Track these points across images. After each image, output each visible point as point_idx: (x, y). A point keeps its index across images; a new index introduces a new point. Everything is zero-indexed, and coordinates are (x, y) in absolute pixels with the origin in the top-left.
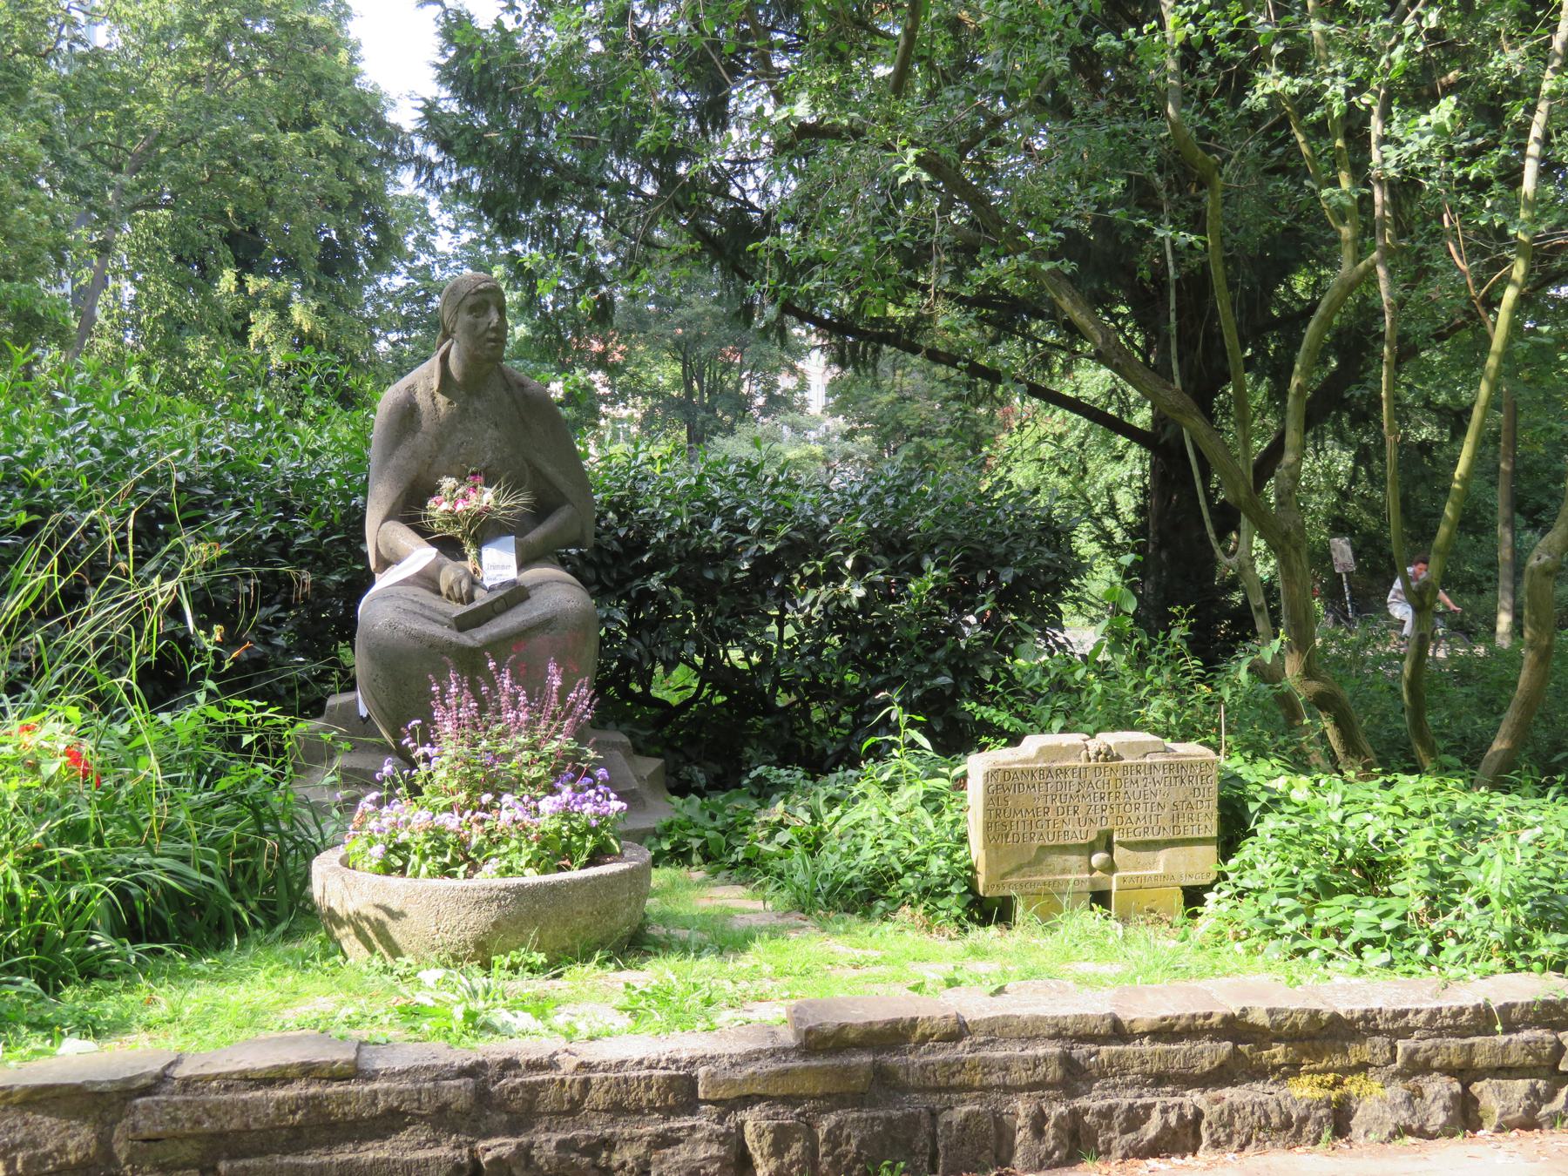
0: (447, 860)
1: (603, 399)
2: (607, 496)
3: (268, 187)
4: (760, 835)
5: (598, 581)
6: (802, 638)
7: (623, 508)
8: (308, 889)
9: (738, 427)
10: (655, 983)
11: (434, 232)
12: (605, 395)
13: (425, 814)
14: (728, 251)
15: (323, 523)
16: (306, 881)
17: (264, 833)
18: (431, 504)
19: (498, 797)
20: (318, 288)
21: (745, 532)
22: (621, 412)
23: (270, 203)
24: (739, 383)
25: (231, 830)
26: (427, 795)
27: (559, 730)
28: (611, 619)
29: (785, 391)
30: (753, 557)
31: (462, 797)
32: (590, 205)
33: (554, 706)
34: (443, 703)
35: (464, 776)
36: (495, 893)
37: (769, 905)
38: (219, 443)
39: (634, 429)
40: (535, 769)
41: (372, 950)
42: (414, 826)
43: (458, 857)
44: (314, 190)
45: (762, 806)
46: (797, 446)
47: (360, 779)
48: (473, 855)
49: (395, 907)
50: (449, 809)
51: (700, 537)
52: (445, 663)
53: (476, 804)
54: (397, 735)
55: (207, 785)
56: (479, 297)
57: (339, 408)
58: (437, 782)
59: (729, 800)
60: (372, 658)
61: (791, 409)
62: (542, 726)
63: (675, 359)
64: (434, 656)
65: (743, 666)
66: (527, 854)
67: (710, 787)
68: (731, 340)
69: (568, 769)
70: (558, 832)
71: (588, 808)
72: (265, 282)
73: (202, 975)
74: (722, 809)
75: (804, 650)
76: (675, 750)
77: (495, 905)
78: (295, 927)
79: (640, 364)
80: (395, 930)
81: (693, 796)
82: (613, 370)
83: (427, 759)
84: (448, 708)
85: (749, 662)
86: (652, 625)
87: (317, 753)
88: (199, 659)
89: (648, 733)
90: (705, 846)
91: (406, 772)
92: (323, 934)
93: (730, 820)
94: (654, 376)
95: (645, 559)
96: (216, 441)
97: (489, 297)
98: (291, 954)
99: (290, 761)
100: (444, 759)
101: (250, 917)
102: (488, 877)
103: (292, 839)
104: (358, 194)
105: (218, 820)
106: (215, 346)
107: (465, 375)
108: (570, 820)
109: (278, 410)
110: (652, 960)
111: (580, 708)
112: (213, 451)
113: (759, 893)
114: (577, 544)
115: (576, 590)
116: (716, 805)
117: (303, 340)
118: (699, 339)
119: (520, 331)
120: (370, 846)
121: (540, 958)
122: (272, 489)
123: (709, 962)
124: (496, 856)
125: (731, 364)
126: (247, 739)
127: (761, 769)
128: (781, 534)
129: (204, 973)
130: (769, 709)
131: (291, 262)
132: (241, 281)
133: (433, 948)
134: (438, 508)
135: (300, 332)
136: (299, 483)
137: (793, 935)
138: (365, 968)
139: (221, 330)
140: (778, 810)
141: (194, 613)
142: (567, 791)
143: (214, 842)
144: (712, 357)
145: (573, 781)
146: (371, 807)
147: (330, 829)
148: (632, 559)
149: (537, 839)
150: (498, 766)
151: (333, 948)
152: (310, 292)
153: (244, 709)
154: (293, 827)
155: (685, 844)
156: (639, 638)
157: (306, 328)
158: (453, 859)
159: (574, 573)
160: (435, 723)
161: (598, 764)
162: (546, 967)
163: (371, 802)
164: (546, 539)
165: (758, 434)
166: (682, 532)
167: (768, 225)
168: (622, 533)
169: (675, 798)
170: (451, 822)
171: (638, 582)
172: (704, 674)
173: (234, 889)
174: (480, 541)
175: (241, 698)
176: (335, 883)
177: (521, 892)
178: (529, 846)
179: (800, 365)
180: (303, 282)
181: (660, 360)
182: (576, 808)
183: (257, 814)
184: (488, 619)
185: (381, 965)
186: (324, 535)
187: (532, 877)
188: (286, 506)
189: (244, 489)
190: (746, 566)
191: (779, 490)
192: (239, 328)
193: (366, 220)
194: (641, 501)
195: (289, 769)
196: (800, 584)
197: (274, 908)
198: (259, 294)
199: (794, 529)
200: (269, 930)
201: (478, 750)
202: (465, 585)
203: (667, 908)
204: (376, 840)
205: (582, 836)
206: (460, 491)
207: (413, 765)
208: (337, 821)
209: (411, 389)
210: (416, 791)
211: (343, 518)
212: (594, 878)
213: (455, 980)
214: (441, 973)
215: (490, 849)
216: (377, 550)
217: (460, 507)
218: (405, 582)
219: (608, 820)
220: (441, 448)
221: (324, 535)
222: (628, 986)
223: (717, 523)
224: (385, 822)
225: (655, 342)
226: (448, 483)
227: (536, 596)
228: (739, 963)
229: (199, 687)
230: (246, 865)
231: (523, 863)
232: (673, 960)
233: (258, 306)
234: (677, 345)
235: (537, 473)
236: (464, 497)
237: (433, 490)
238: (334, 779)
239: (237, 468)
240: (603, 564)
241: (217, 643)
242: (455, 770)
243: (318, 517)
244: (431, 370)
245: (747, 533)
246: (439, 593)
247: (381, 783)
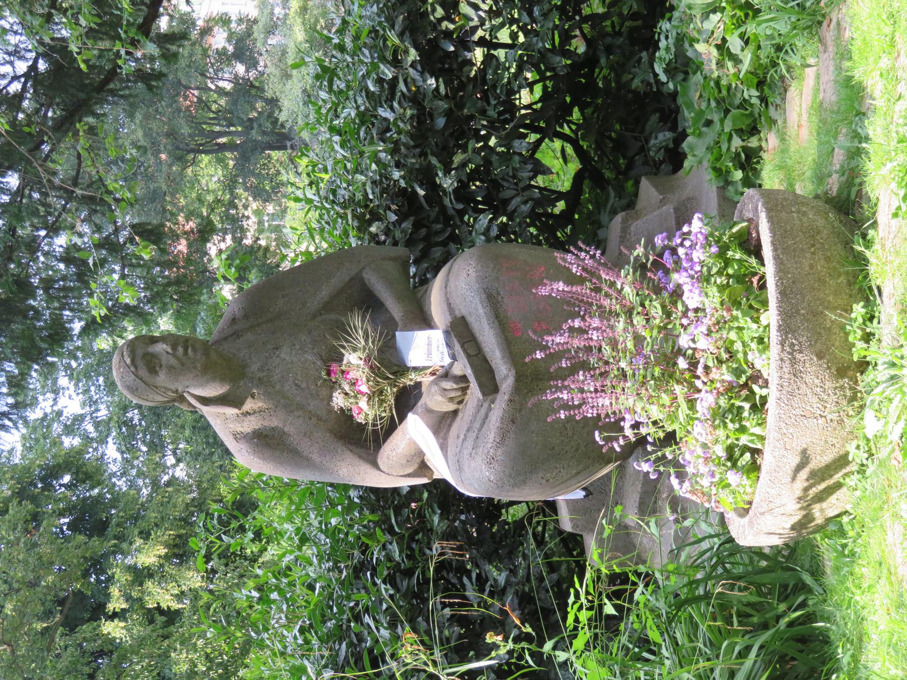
0: (747, 406)
1: (238, 241)
2: (353, 233)
3: (16, 586)
4: (732, 71)
5: (444, 244)
6: (512, 21)
7: (366, 215)
8: (767, 551)
9: (269, 95)
10: (894, 185)
11: (59, 414)
12: (234, 239)
13: (698, 429)
14: (82, 96)
15: (378, 531)
16: (758, 552)
17: (707, 596)
18: (360, 419)
19: (680, 352)
20: (121, 538)
21: (394, 82)
22: (251, 224)
23: (33, 585)
24: (221, 92)
25: (703, 628)
26: (675, 426)
27: (612, 284)
28: (486, 232)
29: (229, 40)
30: (422, 74)
31: (678, 389)
32: (32, 246)
33: (585, 290)
34: (579, 406)
35: (658, 388)
36: (786, 356)
37: (811, 61)
38: (292, 635)
39: (270, 208)
40: (653, 312)
41: (838, 486)
42: (708, 440)
43: (745, 394)
44: (18, 539)
45: (699, 68)
46: (291, 28)
47: (651, 497)
48: (743, 379)
49: (796, 460)
50: (691, 403)
51: (399, 132)
52: (535, 405)
53: (687, 375)
54: (606, 459)
55: (653, 653)
56: (140, 363)
57: (256, 513)
58: (661, 416)
59: (690, 106)
60: (524, 482)
61: (249, 33)
62: (606, 303)
63: (194, 162)
64: (520, 418)
65: (538, 89)
66: (745, 321)
67: (674, 127)
68: (173, 99)
69: (654, 273)
70: (722, 288)
71: (698, 255)
72: (115, 591)
73: (855, 659)
74: (701, 113)
75: (526, 18)
76: (630, 166)
77: (798, 356)
78: (807, 566)
79: (200, 200)
80: (819, 461)
81: (685, 145)
82: (205, 232)
83: (636, 426)
84: (584, 402)
85: (535, 82)
86: (494, 186)
87: (623, 541)
88: (521, 657)
89: (612, 193)
90: (740, 132)
91: (649, 448)
92: (818, 536)
93: (713, 104)
94: (212, 186)
95: (422, 192)
96: (290, 639)
97: (140, 352)
98: (837, 569)
99: (633, 568)
100: (639, 408)
101: (796, 610)
102: (768, 363)
103: (714, 567)
104: (21, 494)
105: (691, 641)
106: (182, 644)
107: (223, 379)
108: (710, 275)
109: (257, 576)
110: (868, 189)
111: (589, 262)
112: (300, 641)
113: (797, 72)
114: (405, 266)
115: (454, 270)
116: (696, 121)
117: (180, 552)
118: (172, 134)
119: (165, 324)
120: (729, 485)
121: (859, 310)
122: (342, 583)
123: (874, 128)
124: (745, 354)
125: (200, 99)
126: (609, 609)
127: (658, 68)
128: (397, 41)
129: (853, 656)
130: (590, 60)
131: (94, 565)
132: (114, 616)
133: (841, 422)
134: (365, 411)
135: (166, 557)
136: (333, 556)
137: (847, 34)
138: (858, 493)
139: (165, 637)
140: (705, 50)
141: (470, 661)
142: (678, 278)
143: (714, 646)
144: (192, 120)
145: (667, 272)
146: (686, 485)
147: (705, 528)
148: (421, 207)
149: (729, 310)
150: (647, 351)
151: (835, 526)
152: (124, 546)
153: (578, 613)
154: (700, 567)
155: (738, 155)
156: (506, 202)
157: (163, 551)
158: (746, 399)
159: (436, 270)
160: (599, 415)
161: (650, 243)
162: (868, 303)
163: (681, 483)
164: (400, 299)
165: (277, 72)
166: (394, 151)
167: (56, 51)
168: (393, 217)
169: (687, 164)
170: (706, 401)
171: (447, 202)
172: (549, 133)
173: (765, 626)
174: (402, 369)
175: (565, 619)
176: (764, 522)
177: (786, 329)
178: (736, 319)
179: (200, 23)
180: (114, 553)
181: (196, 179)
182: (698, 268)
183: (689, 601)
184: (486, 361)
185: (857, 476)
186: (391, 531)
187: (771, 316)
188: (358, 571)
189: (341, 611)
190: (432, 82)
191: (348, 42)
192: (164, 619)
193: (48, 487)
194: (359, 196)
195: (642, 569)
196: (453, 21)
197: (785, 587)
198: (128, 598)
199: (392, 27)
200: (810, 591)
201: (629, 372)
202: (448, 385)
203: (808, 174)
204: (722, 480)
205: (727, 263)
206: (347, 388)
207: (642, 441)
208: (696, 522)
209: (237, 436)
210: (671, 438)
211: (373, 512)
212: (775, 250)
213: (878, 399)
214: (869, 414)
215: (738, 361)
216: (409, 475)
217: (364, 388)
218: (443, 447)
219: (712, 235)
220: (300, 407)
221: (391, 531)
222: (896, 215)
223: (384, 113)
224: (703, 469)
225: (176, 184)
226: (339, 400)
227: (462, 309)
228: (877, 94)
229: (550, 657)
230: (739, 615)
231: (755, 326)
232: (869, 166)
233: (140, 600)
234: (180, 159)
235: (327, 307)
236: (354, 384)
237: (346, 416)
238: (652, 524)
239: (319, 618)
240: (426, 238)
241: (506, 639)
242: (651, 397)
243: (371, 536)
244: (218, 415)
245: (395, 79)
246: (455, 413)
247: (660, 474)
